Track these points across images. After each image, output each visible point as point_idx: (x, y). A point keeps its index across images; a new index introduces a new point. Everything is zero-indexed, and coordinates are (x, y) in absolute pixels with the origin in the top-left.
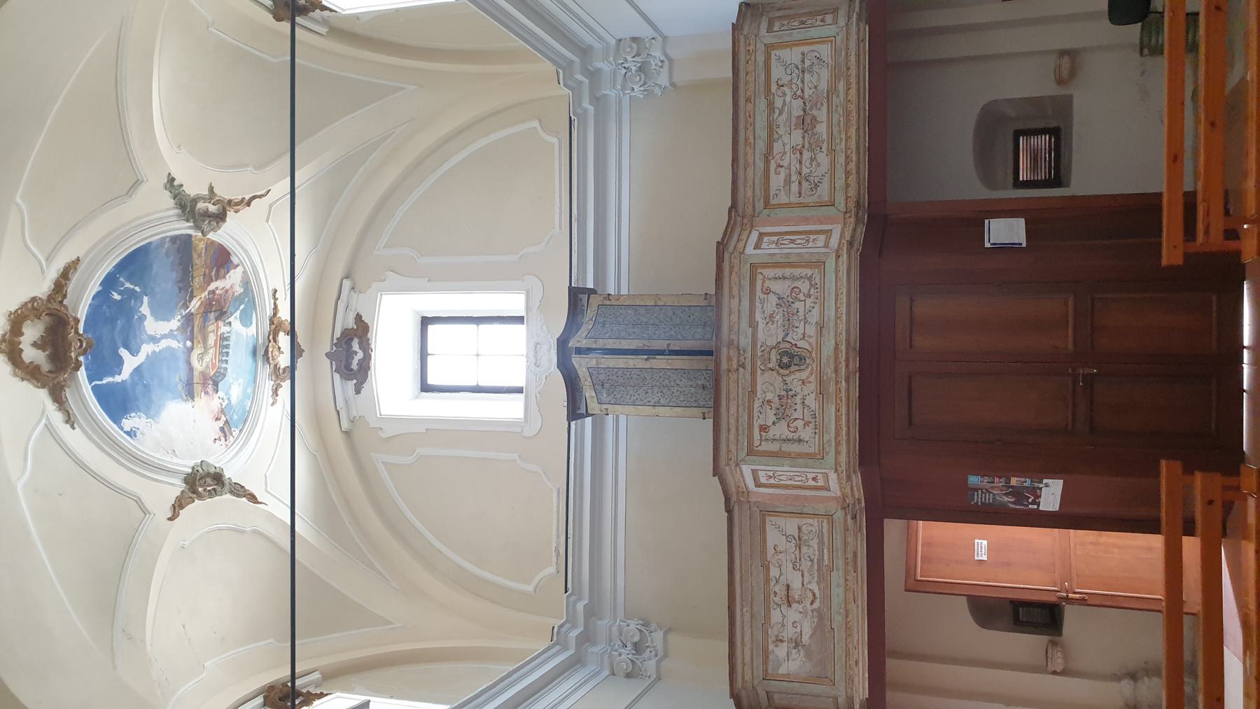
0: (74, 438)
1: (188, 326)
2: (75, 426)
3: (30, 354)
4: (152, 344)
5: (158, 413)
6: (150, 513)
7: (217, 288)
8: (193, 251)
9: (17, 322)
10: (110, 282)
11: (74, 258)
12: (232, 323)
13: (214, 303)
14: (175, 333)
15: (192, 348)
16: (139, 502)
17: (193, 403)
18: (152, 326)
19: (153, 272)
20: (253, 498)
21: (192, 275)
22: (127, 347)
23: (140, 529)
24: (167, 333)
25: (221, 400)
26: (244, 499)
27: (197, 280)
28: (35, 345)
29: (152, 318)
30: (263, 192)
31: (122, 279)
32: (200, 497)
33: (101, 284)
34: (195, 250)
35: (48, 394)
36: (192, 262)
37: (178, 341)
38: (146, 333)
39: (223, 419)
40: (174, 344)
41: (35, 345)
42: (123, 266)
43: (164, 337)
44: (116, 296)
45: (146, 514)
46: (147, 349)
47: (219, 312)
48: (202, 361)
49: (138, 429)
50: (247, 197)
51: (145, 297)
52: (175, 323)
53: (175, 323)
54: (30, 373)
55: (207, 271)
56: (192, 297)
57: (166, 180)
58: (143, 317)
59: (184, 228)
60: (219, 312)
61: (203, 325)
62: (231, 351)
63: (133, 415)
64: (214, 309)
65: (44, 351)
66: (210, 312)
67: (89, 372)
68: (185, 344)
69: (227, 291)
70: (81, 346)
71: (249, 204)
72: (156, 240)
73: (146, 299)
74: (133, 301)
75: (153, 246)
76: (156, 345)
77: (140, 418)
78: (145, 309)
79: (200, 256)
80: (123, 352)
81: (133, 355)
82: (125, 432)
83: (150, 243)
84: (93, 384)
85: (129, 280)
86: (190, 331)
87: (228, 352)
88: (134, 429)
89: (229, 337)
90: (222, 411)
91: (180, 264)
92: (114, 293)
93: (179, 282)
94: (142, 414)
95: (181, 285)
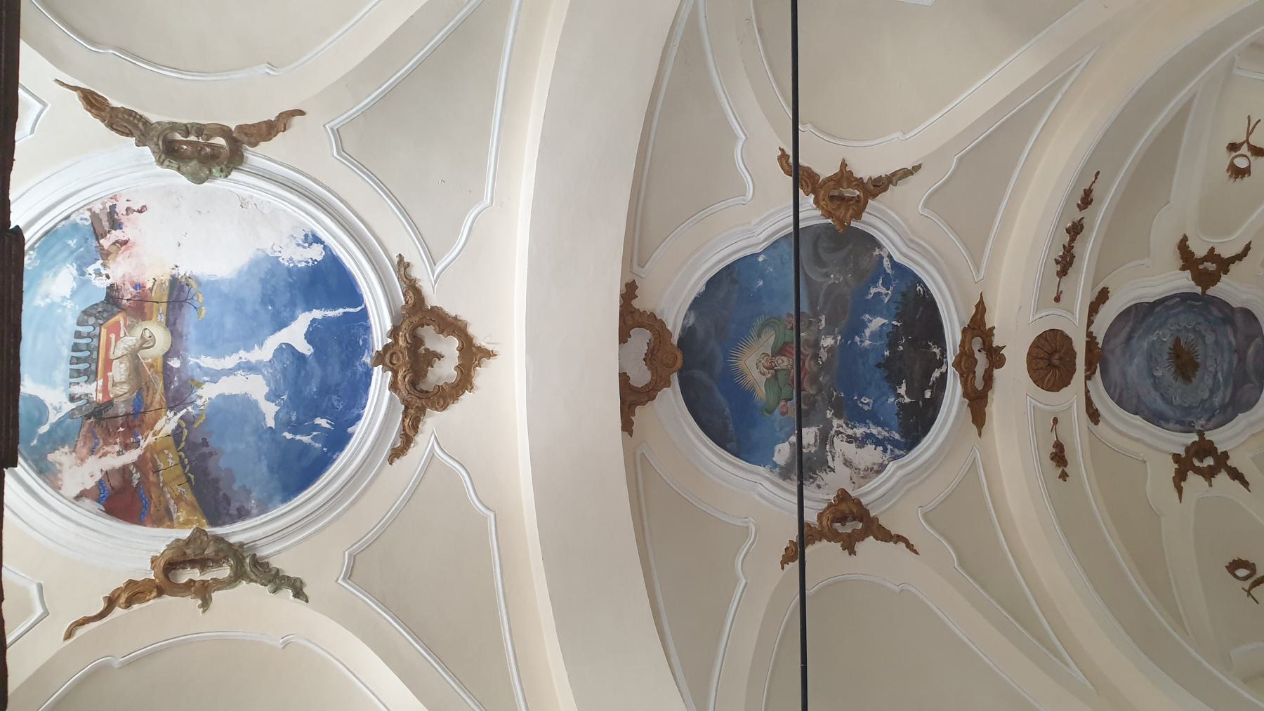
0: (402, 243)
1: (177, 390)
2: (396, 260)
3: (449, 347)
4: (253, 361)
5: (255, 264)
6: (332, 129)
7: (119, 453)
8: (196, 503)
9: (464, 382)
10: (338, 440)
11: (397, 462)
12: (66, 400)
13: (121, 429)
14: (206, 378)
15: (166, 356)
16: (341, 149)
17: (174, 272)
18: (256, 388)
19: (265, 463)
20: (93, 102)
21: (184, 467)
22: (300, 357)
23: (360, 112)
24: (224, 378)
25: (103, 272)
26: (115, 103)
27: (171, 461)
28: (440, 357)
29: (254, 397)
30: (81, 632)
31: (318, 445)
32: (224, 132)
33: (351, 436)
34: (192, 504)
35: (426, 301)
36: (192, 488)
37: (200, 367)
38: (263, 375)
39: (106, 243)
40: (208, 362)
41: (440, 357)
42: (319, 465)
43: (230, 372)
44: (323, 422)
45: (337, 129)
46: (265, 352)
47: (104, 416)
48: (142, 337)
49: (298, 245)
50: (118, 611)
51: (273, 426)
52: (208, 393)
53: (208, 393)
54: (451, 326)
55: (152, 478)
56: (177, 434)
57: (305, 590)
58: (273, 398)
59: (236, 532)
60: (104, 416)
61: (144, 393)
62: (66, 352)
63: (303, 264)
64: (120, 421)
65: (427, 350)
66: (127, 415)
67: (364, 323)
68: (184, 362)
69: (92, 452)
70: (392, 356)
71: (111, 602)
72: (275, 508)
73: (271, 423)
74: (294, 418)
75: (278, 498)
76: (243, 360)
77: (291, 259)
78: (270, 411)
79: (178, 499)
80: (305, 348)
81: (288, 345)
82: (322, 243)
83: (285, 500)
84: (359, 309)
85: (306, 447)
86: (171, 382)
87: (73, 351)
88: (307, 245)
89: (71, 377)
90: (105, 255)
91: (216, 481)
92: (328, 426)
93: (211, 454)
94: (286, 264)
95: (205, 450)
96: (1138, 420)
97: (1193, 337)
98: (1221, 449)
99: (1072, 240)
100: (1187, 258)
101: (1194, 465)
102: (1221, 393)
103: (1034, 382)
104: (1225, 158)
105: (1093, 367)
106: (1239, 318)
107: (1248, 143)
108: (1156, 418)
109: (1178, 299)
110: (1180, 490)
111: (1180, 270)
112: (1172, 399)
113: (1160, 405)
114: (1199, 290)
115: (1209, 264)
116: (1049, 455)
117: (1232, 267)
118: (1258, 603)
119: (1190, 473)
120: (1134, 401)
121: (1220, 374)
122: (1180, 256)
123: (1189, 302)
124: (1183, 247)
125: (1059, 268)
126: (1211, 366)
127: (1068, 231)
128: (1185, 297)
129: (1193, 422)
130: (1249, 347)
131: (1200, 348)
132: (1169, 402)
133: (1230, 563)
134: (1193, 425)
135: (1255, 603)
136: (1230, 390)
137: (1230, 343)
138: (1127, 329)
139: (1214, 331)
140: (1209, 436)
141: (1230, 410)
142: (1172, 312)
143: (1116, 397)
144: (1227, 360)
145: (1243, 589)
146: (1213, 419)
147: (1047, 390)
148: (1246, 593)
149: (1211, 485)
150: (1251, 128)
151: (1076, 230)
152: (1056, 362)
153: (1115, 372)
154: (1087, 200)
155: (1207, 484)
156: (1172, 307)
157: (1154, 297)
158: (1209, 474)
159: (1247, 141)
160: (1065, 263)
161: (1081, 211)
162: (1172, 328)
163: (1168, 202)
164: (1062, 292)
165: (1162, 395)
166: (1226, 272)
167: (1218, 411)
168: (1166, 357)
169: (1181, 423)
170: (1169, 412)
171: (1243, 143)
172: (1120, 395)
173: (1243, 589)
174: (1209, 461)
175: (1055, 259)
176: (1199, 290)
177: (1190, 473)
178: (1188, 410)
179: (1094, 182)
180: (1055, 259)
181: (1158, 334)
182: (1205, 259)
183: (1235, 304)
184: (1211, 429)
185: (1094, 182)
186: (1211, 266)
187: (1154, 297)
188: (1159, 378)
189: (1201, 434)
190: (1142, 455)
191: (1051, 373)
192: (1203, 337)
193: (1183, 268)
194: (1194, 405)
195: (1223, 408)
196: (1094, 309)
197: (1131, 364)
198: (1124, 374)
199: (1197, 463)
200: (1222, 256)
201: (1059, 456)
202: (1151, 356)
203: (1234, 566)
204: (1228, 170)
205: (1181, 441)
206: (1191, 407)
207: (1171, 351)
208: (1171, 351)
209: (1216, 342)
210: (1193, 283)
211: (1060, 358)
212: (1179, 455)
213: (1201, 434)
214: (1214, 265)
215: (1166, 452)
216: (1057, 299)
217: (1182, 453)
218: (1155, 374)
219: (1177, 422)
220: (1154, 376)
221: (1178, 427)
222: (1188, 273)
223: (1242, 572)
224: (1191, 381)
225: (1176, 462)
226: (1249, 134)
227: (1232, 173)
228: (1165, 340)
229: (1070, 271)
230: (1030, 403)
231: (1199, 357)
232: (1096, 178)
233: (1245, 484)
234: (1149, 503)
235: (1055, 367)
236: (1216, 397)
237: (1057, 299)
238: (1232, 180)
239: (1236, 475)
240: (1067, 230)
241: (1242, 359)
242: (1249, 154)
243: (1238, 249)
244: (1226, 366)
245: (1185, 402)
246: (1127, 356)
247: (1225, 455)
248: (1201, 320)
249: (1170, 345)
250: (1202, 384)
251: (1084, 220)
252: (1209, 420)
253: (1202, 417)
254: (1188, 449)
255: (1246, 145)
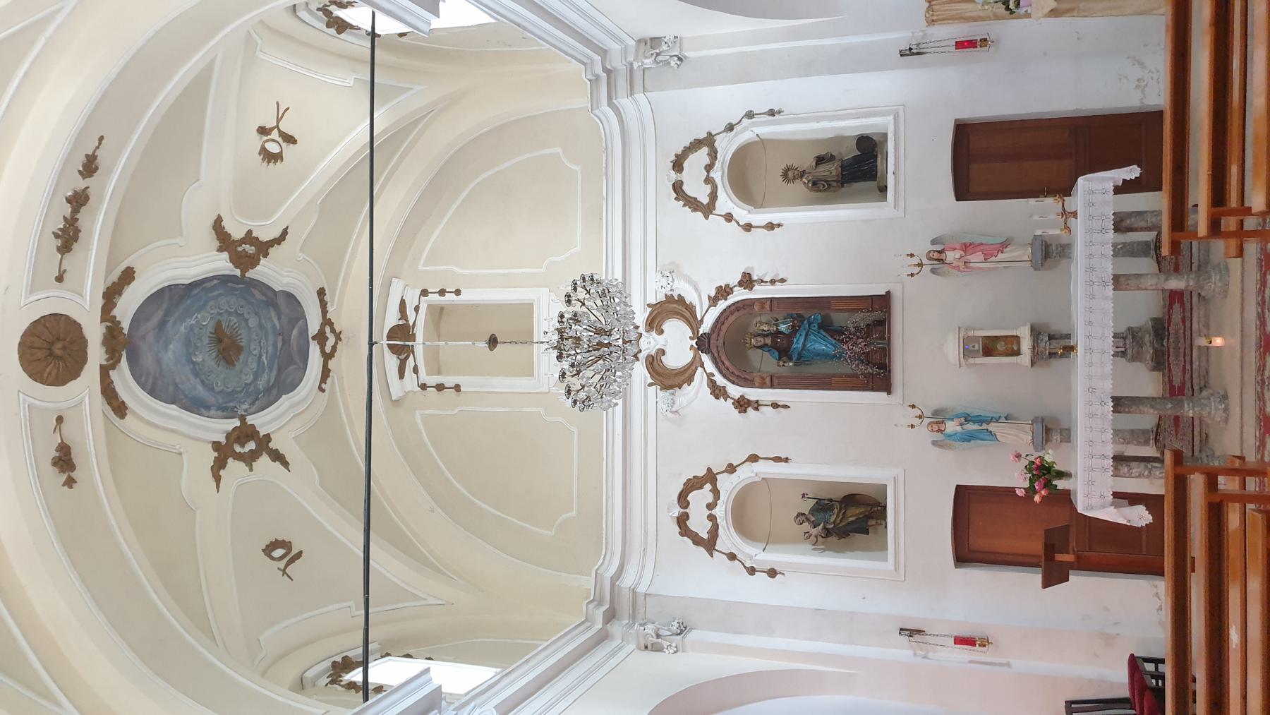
96: (173, 410)
97: (235, 320)
98: (262, 432)
99: (76, 211)
100: (224, 240)
101: (235, 451)
102: (265, 375)
103: (30, 377)
104: (256, 141)
105: (117, 355)
106: (281, 301)
107: (279, 129)
108: (195, 406)
109: (216, 282)
110: (217, 479)
111: (218, 251)
112: (213, 383)
113: (200, 391)
114: (238, 272)
115: (248, 246)
116: (50, 461)
117: (272, 251)
118: (292, 580)
119: (230, 460)
120: (171, 388)
121: (264, 357)
122: (215, 236)
123: (229, 284)
124: (218, 226)
125: (59, 242)
126: (255, 349)
127: (69, 200)
128: (225, 280)
129: (236, 407)
130: (293, 330)
131: (243, 331)
132: (210, 388)
133: (267, 546)
134: (236, 409)
135: (290, 580)
136: (274, 373)
137: (274, 326)
138: (160, 313)
139: (256, 314)
140: (250, 420)
141: (274, 392)
142: (210, 295)
143: (149, 386)
144: (272, 342)
145: (279, 569)
146: (257, 402)
147: (48, 385)
148: (281, 573)
149: (251, 470)
150: (280, 116)
151: (79, 200)
152: (59, 352)
153: (147, 360)
154: (90, 167)
155: (248, 469)
156: (215, 288)
157: (189, 279)
158: (249, 459)
159: (277, 126)
160: (68, 237)
161: (84, 179)
162: (212, 312)
163: (198, 180)
164: (65, 271)
165: (202, 382)
166: (266, 256)
167: (262, 394)
168: (206, 341)
169: (224, 409)
170: (211, 400)
171: (273, 128)
172: (154, 384)
173: (279, 569)
174: (251, 445)
175: (53, 233)
176: (238, 272)
177: (230, 460)
178: (231, 395)
179: (98, 148)
180: (53, 233)
181: (197, 317)
182: (242, 241)
183: (277, 288)
184: (254, 413)
185: (98, 148)
186: (250, 249)
187: (189, 279)
188: (198, 364)
189: (243, 419)
190: (178, 447)
191: (52, 365)
192: (246, 320)
193: (220, 250)
194: (237, 389)
195: (268, 390)
196: (112, 295)
197: (167, 351)
198: (158, 361)
199: (238, 449)
200: (260, 239)
201: (64, 460)
202: (190, 341)
203: (269, 550)
204: (260, 154)
205: (220, 428)
206: (235, 392)
207: (211, 335)
208: (211, 335)
209: (260, 326)
210: (231, 265)
211: (64, 348)
212: (219, 443)
213: (243, 419)
214: (253, 248)
215: (204, 441)
216: (60, 279)
217: (222, 439)
218: (194, 360)
219: (219, 408)
220: (193, 363)
221: (219, 413)
222: (225, 255)
223: (278, 553)
224: (234, 365)
225: (215, 450)
226: (278, 121)
227: (264, 156)
228: (204, 323)
229: (75, 246)
230: (24, 400)
231: (243, 340)
232: (100, 144)
233: (285, 464)
234: (184, 500)
235: (57, 357)
236: (261, 380)
237: (60, 279)
238: (265, 164)
239: (277, 457)
240: (66, 199)
241: (286, 342)
242: (280, 140)
243: (276, 233)
244: (270, 349)
245: (228, 388)
246: (161, 342)
247: (268, 437)
248: (243, 303)
249: (210, 328)
250: (246, 368)
251: (88, 190)
252: (252, 404)
253: (245, 401)
254: (228, 436)
255: (276, 129)
